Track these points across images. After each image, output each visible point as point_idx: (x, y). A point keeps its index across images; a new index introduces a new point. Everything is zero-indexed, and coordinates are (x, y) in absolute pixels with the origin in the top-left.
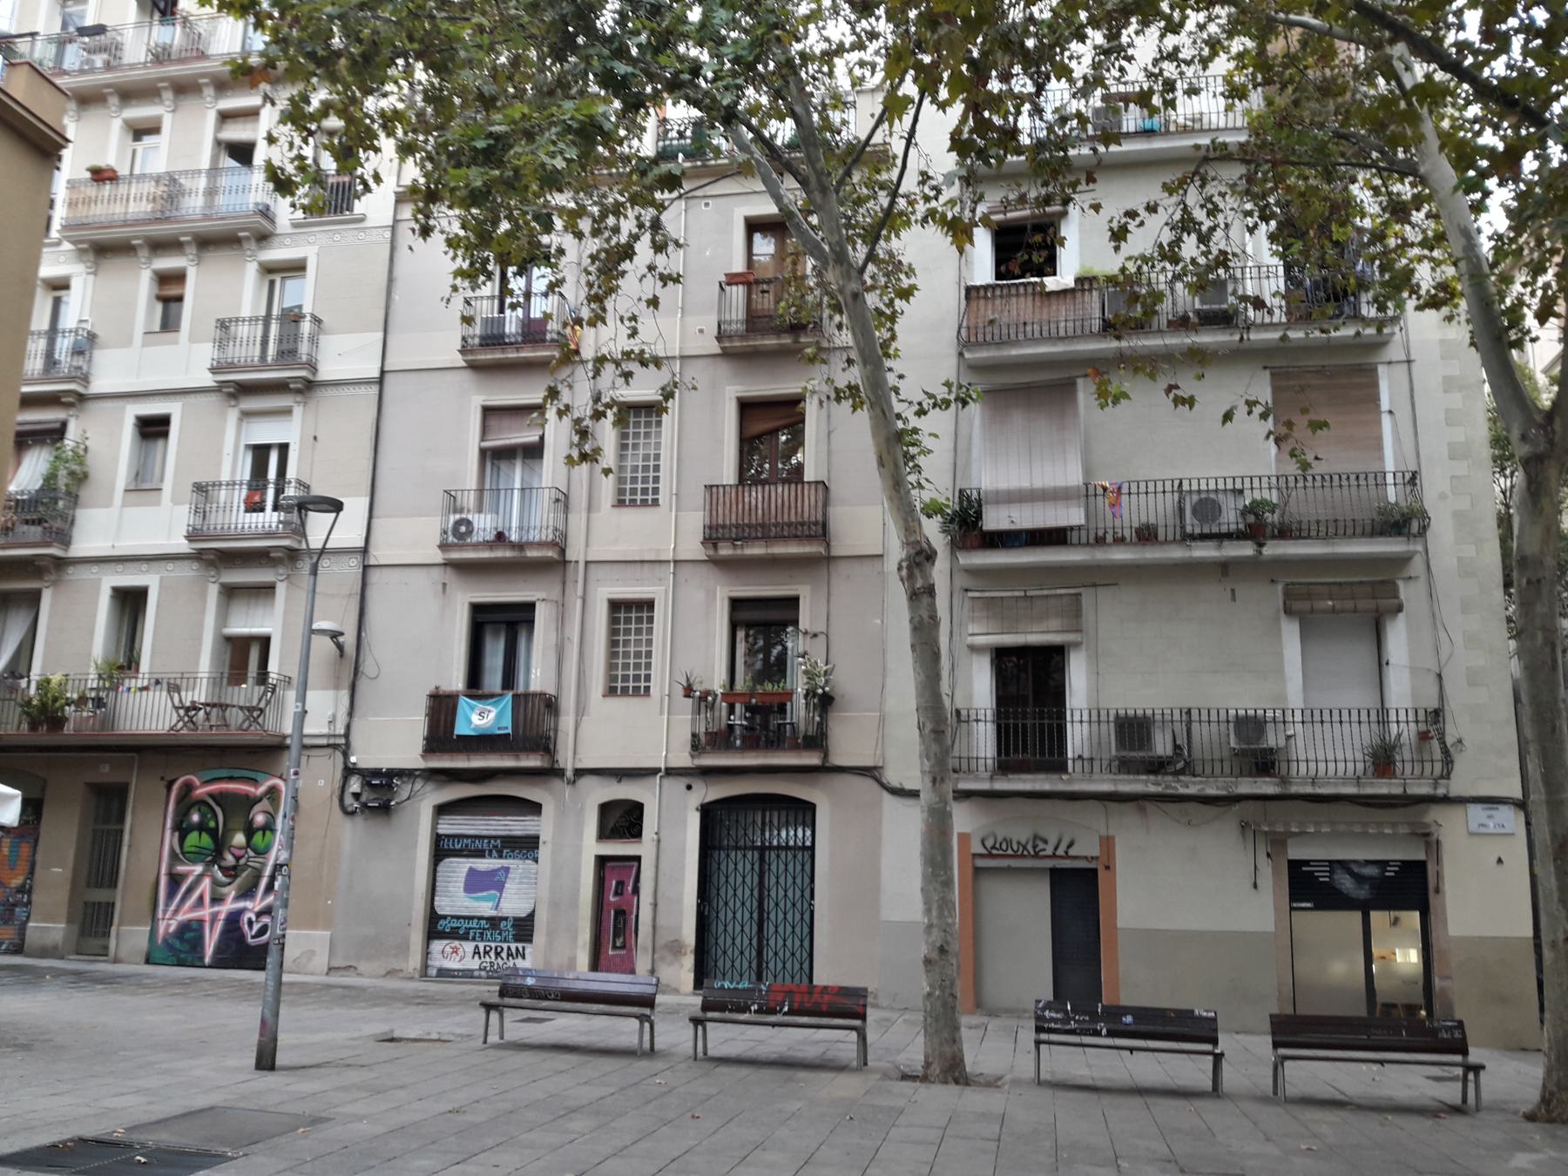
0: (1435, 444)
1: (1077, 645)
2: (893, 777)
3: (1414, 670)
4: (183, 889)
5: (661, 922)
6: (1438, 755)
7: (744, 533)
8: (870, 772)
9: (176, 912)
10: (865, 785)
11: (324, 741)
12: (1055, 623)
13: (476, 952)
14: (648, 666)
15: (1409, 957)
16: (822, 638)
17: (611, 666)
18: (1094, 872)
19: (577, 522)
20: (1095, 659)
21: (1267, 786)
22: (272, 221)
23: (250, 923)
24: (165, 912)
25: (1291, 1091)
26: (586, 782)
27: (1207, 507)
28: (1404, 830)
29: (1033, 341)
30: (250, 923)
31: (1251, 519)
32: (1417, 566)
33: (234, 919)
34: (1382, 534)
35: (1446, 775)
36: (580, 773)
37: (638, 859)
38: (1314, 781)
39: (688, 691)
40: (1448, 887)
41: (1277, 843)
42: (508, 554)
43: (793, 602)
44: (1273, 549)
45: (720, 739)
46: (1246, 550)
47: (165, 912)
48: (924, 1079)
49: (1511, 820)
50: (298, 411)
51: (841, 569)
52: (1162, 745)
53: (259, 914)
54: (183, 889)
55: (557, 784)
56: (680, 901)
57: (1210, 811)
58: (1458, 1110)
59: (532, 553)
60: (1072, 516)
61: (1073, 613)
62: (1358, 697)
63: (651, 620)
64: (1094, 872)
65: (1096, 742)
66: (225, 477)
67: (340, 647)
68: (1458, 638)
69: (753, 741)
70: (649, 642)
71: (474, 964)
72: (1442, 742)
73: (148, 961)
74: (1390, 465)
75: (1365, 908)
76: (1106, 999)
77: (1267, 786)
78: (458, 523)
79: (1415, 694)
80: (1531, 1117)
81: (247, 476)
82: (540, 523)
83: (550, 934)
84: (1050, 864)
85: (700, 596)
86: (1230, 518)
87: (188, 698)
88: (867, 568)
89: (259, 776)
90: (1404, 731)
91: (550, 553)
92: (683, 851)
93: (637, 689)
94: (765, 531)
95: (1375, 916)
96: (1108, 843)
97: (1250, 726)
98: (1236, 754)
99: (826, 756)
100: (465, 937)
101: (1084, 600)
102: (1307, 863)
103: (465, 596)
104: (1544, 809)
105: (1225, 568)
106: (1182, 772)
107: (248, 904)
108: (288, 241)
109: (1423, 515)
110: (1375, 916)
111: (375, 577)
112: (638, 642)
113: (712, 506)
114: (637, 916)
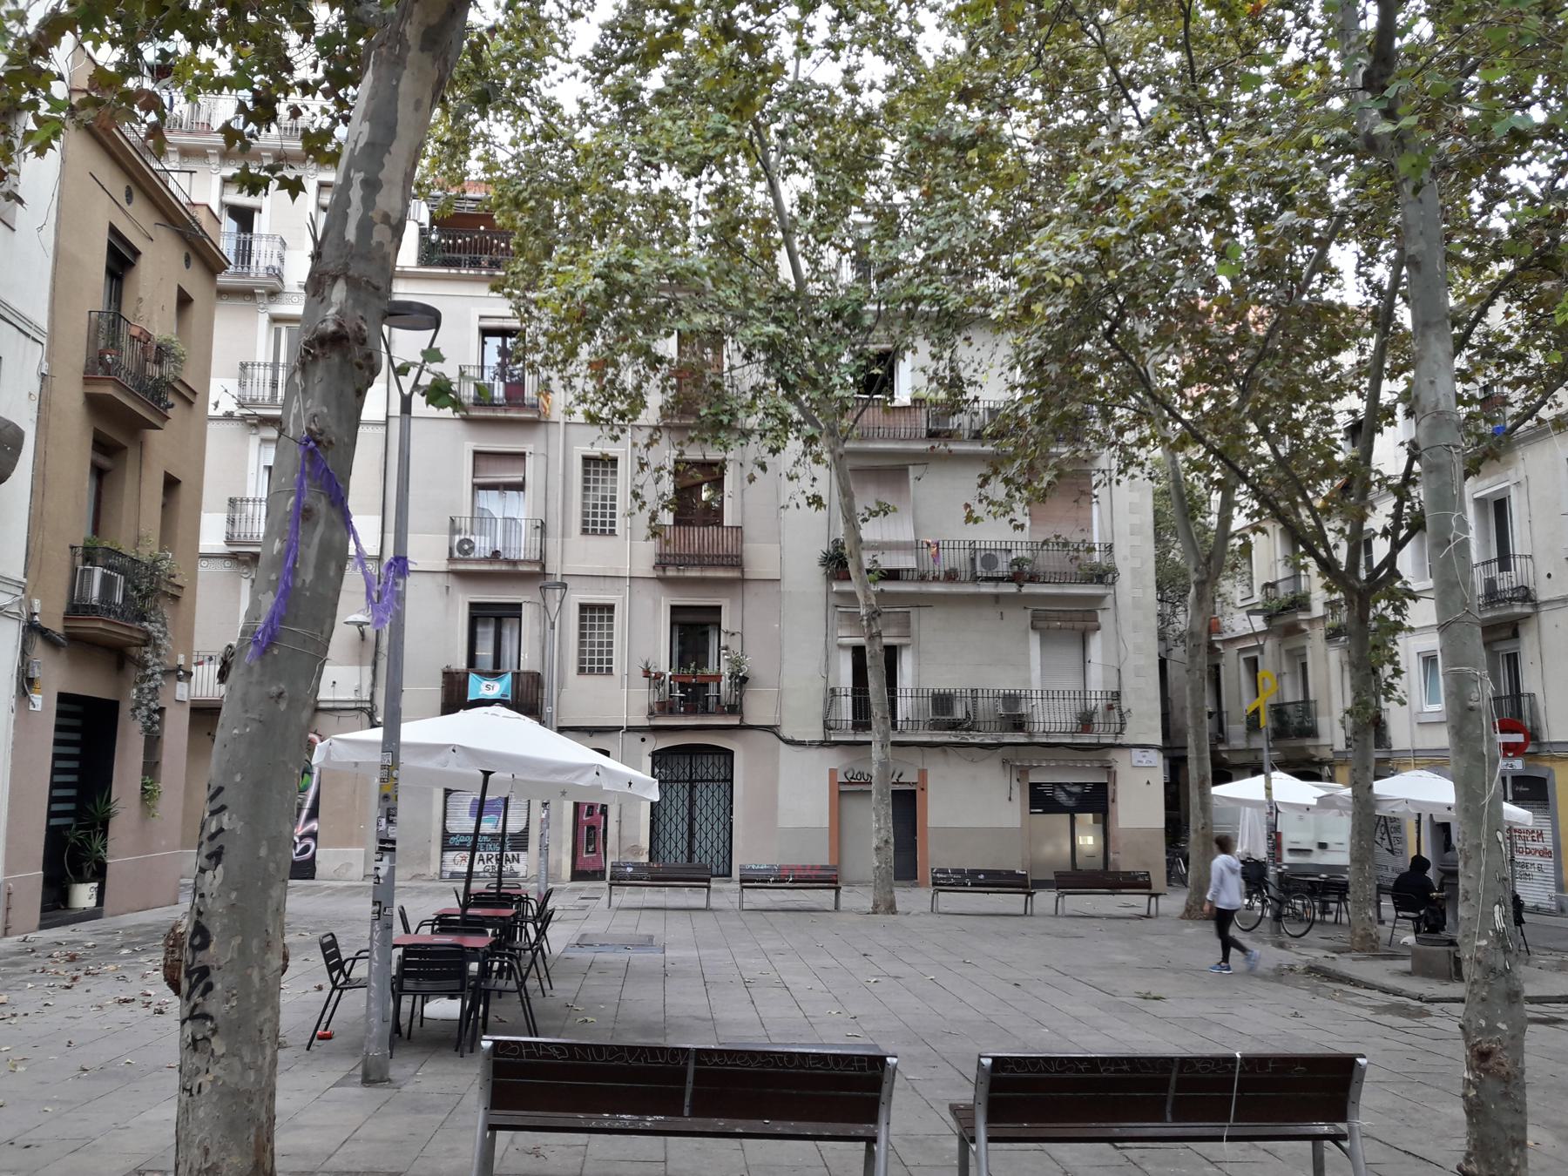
0: (1123, 524)
1: (907, 645)
2: (786, 732)
5: (625, 833)
6: (1118, 720)
7: (682, 561)
10: (771, 737)
11: (352, 705)
14: (610, 652)
15: (1088, 841)
16: (738, 637)
19: (553, 545)
20: (917, 656)
21: (1020, 738)
25: (1068, 912)
27: (990, 561)
28: (1097, 764)
29: (883, 439)
32: (1108, 602)
35: (1121, 733)
38: (1047, 733)
39: (647, 673)
40: (1120, 798)
41: (1024, 772)
42: (504, 568)
43: (718, 609)
44: (1029, 589)
45: (665, 708)
46: (1011, 588)
51: (751, 590)
52: (959, 713)
56: (638, 818)
57: (986, 752)
58: (1140, 917)
60: (906, 561)
61: (905, 625)
62: (1070, 683)
63: (611, 619)
66: (250, 495)
67: (362, 634)
68: (1130, 648)
70: (610, 635)
75: (1072, 811)
77: (1020, 738)
78: (462, 542)
79: (1105, 682)
80: (1182, 918)
82: (522, 547)
85: (649, 602)
86: (1003, 568)
88: (769, 587)
90: (1097, 703)
93: (600, 669)
94: (700, 561)
96: (923, 774)
97: (1012, 700)
98: (1002, 718)
99: (741, 720)
102: (1039, 784)
103: (464, 598)
105: (997, 598)
106: (968, 729)
112: (601, 635)
114: (605, 831)
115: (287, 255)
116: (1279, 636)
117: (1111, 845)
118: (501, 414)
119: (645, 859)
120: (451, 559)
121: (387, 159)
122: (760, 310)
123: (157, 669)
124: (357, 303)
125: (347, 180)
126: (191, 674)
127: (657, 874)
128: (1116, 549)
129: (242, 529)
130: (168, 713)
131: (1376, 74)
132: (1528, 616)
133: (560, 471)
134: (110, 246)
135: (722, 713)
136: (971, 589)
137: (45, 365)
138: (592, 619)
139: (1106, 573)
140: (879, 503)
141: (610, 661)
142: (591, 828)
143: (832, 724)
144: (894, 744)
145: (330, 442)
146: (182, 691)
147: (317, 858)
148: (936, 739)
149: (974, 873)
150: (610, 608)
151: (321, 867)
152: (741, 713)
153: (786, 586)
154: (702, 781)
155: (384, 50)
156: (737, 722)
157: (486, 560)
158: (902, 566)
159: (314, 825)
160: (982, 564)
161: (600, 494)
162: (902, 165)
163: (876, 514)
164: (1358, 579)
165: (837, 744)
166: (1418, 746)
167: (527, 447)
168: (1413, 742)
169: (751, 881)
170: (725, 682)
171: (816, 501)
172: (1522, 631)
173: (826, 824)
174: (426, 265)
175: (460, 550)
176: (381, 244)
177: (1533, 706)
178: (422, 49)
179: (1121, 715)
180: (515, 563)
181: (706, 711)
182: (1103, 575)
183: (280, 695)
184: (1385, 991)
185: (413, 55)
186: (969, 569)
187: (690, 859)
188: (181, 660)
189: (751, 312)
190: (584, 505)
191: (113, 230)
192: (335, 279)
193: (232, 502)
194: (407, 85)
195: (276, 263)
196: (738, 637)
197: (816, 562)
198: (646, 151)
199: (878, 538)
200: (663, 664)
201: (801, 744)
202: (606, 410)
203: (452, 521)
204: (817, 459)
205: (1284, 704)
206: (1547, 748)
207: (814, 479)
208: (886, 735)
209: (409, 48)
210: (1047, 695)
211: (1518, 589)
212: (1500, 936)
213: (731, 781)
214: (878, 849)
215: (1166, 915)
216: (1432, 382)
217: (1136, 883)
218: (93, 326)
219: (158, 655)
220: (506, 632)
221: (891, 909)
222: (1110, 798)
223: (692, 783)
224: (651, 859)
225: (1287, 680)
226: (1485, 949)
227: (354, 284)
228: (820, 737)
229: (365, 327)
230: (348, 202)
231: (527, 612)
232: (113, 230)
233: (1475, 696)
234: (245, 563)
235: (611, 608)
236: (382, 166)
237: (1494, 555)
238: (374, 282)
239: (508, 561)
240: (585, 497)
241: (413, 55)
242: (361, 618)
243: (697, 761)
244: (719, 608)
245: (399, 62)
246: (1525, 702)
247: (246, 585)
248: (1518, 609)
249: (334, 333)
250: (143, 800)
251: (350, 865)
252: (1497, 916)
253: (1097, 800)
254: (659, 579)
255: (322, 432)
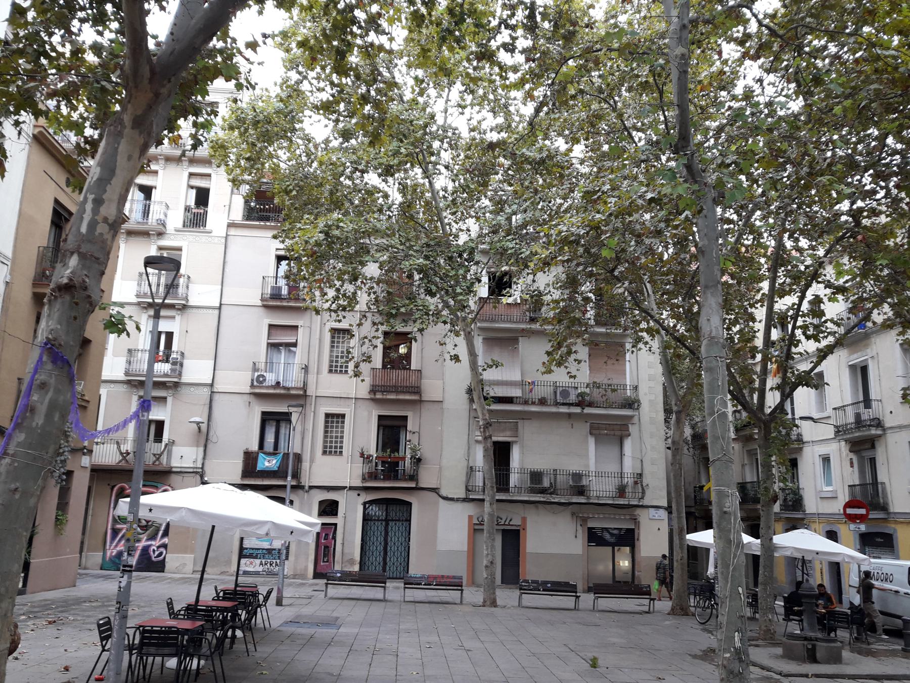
0: (644, 374)
1: (516, 442)
2: (444, 493)
3: (633, 458)
4: (120, 535)
5: (346, 551)
6: (640, 490)
7: (385, 389)
8: (435, 490)
9: (116, 546)
10: (434, 495)
11: (191, 470)
12: (508, 433)
13: (261, 564)
14: (342, 442)
15: (625, 564)
16: (417, 434)
17: (325, 442)
18: (519, 531)
19: (312, 379)
20: (522, 448)
21: (582, 500)
22: (165, 227)
23: (154, 551)
24: (110, 546)
25: (600, 608)
26: (313, 491)
27: (565, 393)
28: (628, 517)
29: (504, 321)
30: (154, 551)
31: (580, 398)
32: (636, 420)
33: (146, 549)
34: (625, 407)
35: (642, 498)
36: (311, 487)
37: (336, 525)
38: (598, 497)
39: (362, 455)
40: (642, 538)
41: (584, 520)
42: (282, 392)
43: (405, 418)
44: (588, 410)
45: (373, 476)
46: (577, 410)
47: (110, 546)
48: (484, 606)
49: (663, 514)
50: (178, 318)
51: (425, 406)
52: (546, 483)
53: (158, 547)
54: (120, 535)
55: (300, 492)
56: (354, 542)
57: (562, 508)
58: (647, 612)
59: (293, 392)
60: (516, 392)
61: (515, 430)
62: (613, 468)
63: (343, 422)
64: (519, 531)
65: (521, 480)
66: (141, 347)
67: (199, 428)
68: (649, 447)
69: (387, 478)
70: (342, 432)
71: (260, 569)
72: (642, 485)
73: (101, 569)
74: (628, 383)
75: (613, 545)
76: (521, 578)
77: (582, 500)
78: (259, 376)
79: (633, 467)
80: (669, 614)
81: (148, 347)
82: (293, 379)
83: (297, 557)
84: (502, 528)
85: (366, 414)
86: (573, 398)
87: (124, 448)
88: (436, 406)
89: (159, 485)
90: (628, 480)
91: (301, 392)
92: (355, 522)
93: (336, 452)
94: (396, 389)
95: (616, 548)
96: (524, 520)
97: (577, 476)
98: (571, 487)
99: (417, 484)
100: (256, 557)
101: (520, 424)
102: (594, 528)
103: (258, 409)
104: (630, 459)
105: (570, 415)
106: (551, 494)
107: (153, 543)
108: (172, 237)
109: (638, 401)
110: (616, 548)
111: (216, 397)
112: (337, 432)
113: (374, 377)
114: (334, 549)
115: (169, 213)
116: (742, 441)
117: (636, 567)
118: (285, 304)
119: (356, 568)
120: (252, 386)
121: (108, 188)
122: (417, 251)
123: (66, 449)
124: (84, 267)
125: (86, 199)
126: (92, 451)
127: (364, 577)
128: (640, 388)
129: (135, 367)
130: (75, 474)
131: (680, 146)
132: (880, 436)
133: (318, 336)
134: (55, 210)
135: (405, 480)
136: (554, 409)
137: (9, 277)
138: (332, 422)
139: (633, 403)
140: (493, 360)
141: (341, 447)
142: (326, 547)
143: (470, 488)
144: (498, 501)
145: (60, 345)
146: (85, 461)
147: (167, 560)
148: (532, 499)
149: (545, 583)
150: (343, 416)
151: (168, 566)
152: (417, 482)
153: (445, 405)
154: (392, 520)
155: (112, 128)
156: (414, 485)
157: (272, 387)
158: (513, 395)
159: (166, 540)
160: (561, 396)
161: (340, 350)
162: (510, 172)
163: (491, 367)
164: (764, 414)
165: (473, 500)
166: (821, 512)
167: (299, 323)
168: (817, 509)
169: (410, 583)
170: (408, 461)
171: (456, 358)
172: (877, 444)
173: (465, 548)
174: (247, 220)
175: (258, 380)
176: (101, 234)
177: (884, 489)
178: (133, 128)
179: (643, 489)
180: (288, 389)
181: (396, 478)
182: (632, 404)
183: (16, 489)
184: (763, 668)
185: (127, 131)
186: (553, 397)
187: (384, 570)
188: (86, 444)
189: (411, 252)
190: (331, 356)
191: (57, 201)
192: (72, 253)
193: (130, 351)
194: (123, 147)
195: (162, 217)
196: (417, 434)
197: (464, 392)
198: (355, 162)
199: (500, 378)
200: (372, 450)
201: (452, 499)
202: (334, 305)
203: (254, 364)
204: (457, 334)
205: (746, 483)
206: (892, 516)
207: (456, 345)
208: (493, 497)
209: (125, 127)
210: (598, 474)
211: (874, 419)
212: (738, 652)
213: (410, 521)
214: (486, 566)
215: (659, 612)
216: (708, 320)
217: (641, 591)
218: (41, 255)
219: (67, 442)
220: (283, 431)
221: (494, 604)
222: (636, 537)
223: (387, 521)
224: (361, 569)
225: (747, 469)
226: (729, 659)
227: (83, 256)
228: (463, 496)
229: (87, 280)
230: (84, 211)
231: (294, 418)
232: (57, 201)
233: (727, 505)
234: (135, 386)
235: (343, 416)
236: (105, 191)
237: (861, 399)
238: (96, 255)
239: (284, 388)
240: (331, 351)
241: (127, 131)
242: (198, 419)
243: (391, 508)
244: (407, 417)
245: (119, 135)
246: (880, 486)
247: (135, 398)
248: (874, 431)
249: (66, 284)
250: (56, 525)
251: (185, 564)
252: (736, 639)
253: (628, 538)
254: (372, 399)
255: (55, 339)
